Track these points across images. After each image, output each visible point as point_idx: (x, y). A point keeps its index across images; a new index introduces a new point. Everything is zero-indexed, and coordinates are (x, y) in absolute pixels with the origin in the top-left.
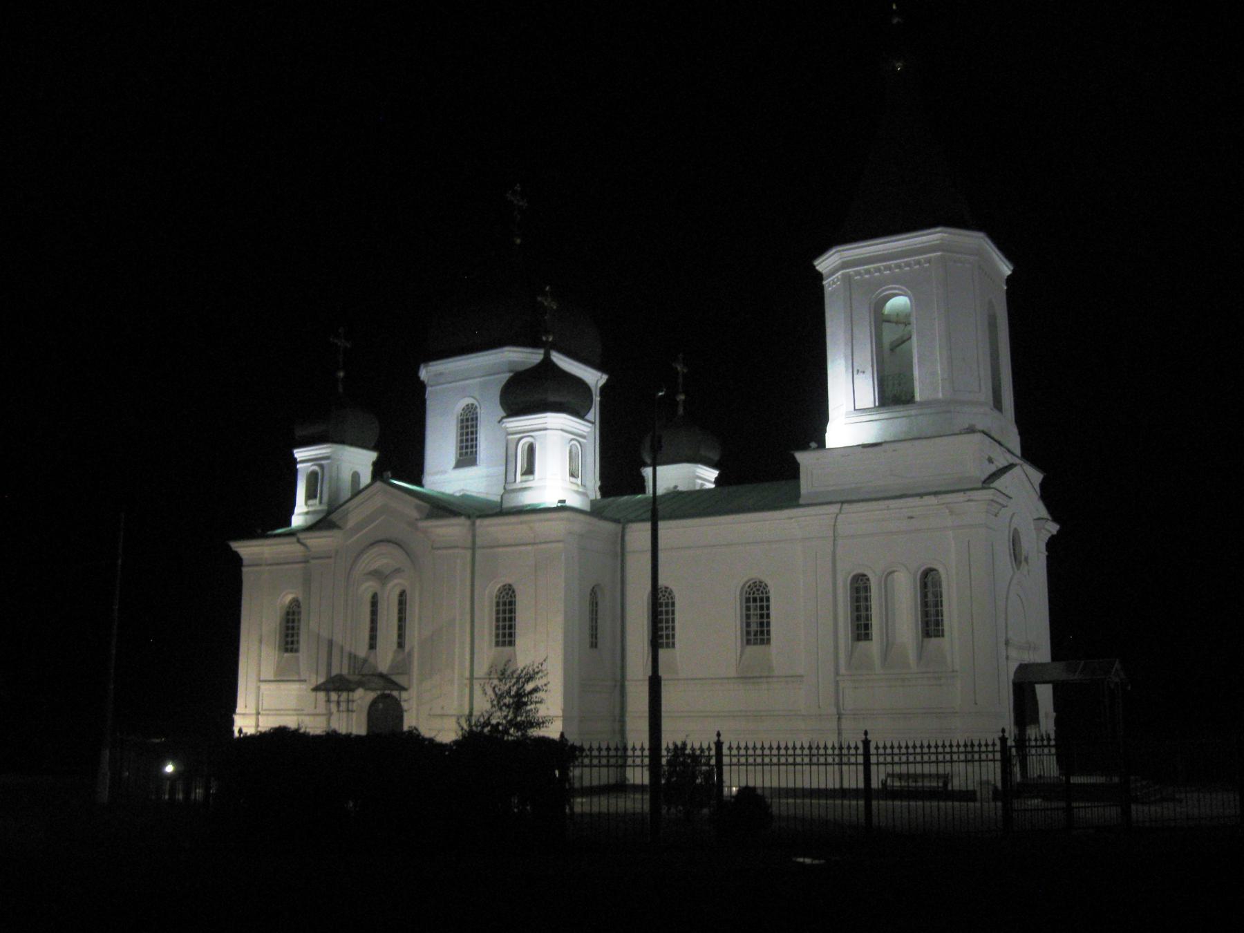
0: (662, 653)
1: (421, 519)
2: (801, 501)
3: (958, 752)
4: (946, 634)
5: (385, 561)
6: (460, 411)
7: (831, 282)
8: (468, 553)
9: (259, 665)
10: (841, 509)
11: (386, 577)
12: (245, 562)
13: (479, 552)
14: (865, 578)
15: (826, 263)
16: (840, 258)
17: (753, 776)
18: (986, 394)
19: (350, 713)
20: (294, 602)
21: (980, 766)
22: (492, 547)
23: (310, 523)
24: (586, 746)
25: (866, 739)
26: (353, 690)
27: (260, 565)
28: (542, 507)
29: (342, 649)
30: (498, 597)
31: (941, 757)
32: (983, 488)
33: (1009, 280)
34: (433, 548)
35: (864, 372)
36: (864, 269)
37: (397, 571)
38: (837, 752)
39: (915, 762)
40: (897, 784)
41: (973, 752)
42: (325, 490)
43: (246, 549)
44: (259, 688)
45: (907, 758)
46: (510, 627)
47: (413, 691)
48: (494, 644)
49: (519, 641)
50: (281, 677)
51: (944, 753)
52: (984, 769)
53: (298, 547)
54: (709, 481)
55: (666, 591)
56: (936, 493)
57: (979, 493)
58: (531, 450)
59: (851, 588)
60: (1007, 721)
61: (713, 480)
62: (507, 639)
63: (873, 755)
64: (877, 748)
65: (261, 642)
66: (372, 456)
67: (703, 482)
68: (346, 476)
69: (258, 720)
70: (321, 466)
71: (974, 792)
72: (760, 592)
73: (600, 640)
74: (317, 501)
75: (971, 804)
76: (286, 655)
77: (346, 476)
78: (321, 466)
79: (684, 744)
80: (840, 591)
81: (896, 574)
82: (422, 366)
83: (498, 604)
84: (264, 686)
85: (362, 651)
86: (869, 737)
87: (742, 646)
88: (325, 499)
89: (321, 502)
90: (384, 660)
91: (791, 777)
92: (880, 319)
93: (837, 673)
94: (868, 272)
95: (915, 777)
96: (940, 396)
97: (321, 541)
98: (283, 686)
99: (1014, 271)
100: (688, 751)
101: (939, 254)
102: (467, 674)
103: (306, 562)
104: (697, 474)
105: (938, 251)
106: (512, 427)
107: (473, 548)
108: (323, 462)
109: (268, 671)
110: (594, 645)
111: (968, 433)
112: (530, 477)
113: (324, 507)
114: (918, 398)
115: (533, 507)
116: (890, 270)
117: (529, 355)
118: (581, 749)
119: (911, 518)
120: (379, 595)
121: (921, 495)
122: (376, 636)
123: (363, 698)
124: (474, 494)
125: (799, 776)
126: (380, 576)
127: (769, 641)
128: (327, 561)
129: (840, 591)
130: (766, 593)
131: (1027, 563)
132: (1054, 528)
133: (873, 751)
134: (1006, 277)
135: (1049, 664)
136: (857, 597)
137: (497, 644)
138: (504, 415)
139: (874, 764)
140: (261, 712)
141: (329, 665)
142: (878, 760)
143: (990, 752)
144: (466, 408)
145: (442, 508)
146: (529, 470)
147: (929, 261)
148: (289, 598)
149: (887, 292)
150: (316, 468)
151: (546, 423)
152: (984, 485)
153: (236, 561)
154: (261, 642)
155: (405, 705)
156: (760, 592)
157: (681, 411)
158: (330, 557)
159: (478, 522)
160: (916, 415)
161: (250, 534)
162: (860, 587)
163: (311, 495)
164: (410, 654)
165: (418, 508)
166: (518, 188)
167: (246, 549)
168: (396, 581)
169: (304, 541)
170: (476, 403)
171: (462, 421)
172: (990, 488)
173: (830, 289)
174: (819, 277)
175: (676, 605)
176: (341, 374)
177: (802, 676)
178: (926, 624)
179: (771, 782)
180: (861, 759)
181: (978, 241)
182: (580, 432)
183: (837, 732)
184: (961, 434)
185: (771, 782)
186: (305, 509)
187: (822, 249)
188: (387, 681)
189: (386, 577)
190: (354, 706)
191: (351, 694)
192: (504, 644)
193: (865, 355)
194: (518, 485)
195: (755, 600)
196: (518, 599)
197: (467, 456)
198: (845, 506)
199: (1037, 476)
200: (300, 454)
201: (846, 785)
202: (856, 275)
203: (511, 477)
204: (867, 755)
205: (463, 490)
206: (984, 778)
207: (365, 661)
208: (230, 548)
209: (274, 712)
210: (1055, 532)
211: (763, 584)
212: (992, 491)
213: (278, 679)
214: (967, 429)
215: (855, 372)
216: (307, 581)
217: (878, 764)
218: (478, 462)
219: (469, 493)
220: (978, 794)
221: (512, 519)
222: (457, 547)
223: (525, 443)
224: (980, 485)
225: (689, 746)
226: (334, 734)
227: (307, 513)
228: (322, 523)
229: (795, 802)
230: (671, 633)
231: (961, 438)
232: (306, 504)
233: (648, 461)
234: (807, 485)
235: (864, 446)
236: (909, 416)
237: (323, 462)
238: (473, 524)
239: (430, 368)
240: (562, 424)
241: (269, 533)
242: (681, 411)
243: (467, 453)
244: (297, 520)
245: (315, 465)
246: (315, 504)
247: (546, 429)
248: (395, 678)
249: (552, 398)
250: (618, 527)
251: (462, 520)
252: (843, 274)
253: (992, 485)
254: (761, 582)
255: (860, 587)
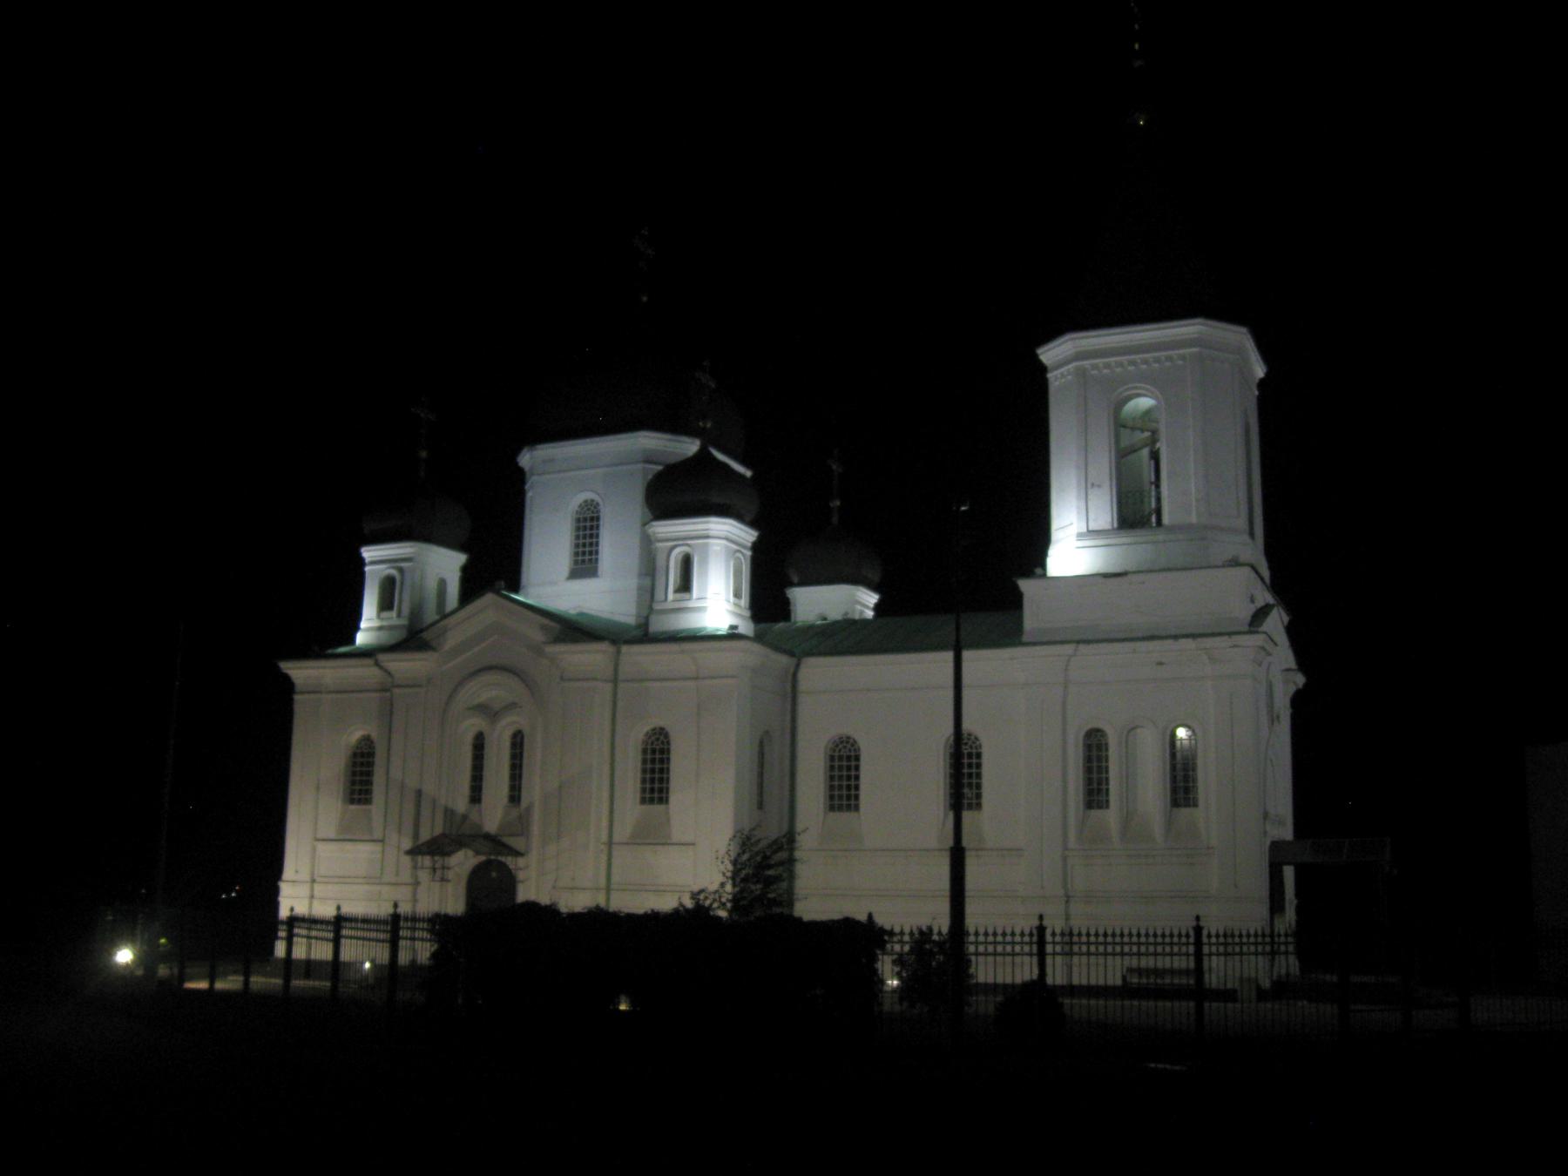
0: (967, 816)
1: (549, 643)
2: (1025, 638)
3: (986, 943)
4: (1201, 802)
5: (494, 693)
6: (576, 508)
7: (1066, 373)
8: (609, 687)
9: (316, 819)
10: (1075, 650)
11: (496, 714)
12: (298, 688)
13: (621, 685)
14: (1100, 734)
15: (1049, 354)
16: (1074, 347)
17: (1011, 970)
18: (1242, 522)
19: (444, 883)
20: (364, 740)
21: (1241, 961)
22: (642, 680)
23: (393, 641)
24: (897, 930)
25: (1041, 924)
26: (449, 854)
27: (320, 692)
28: (703, 633)
29: (434, 802)
30: (645, 742)
31: (1126, 949)
32: (1251, 632)
33: (1262, 384)
34: (562, 679)
35: (1099, 486)
36: (1140, 358)
37: (512, 706)
38: (1268, 939)
39: (1147, 954)
40: (1135, 980)
41: (1071, 943)
42: (405, 600)
43: (300, 672)
44: (314, 850)
45: (1013, 948)
46: (661, 780)
47: (533, 858)
48: (638, 800)
49: (675, 797)
50: (346, 835)
51: (1131, 944)
52: (1245, 964)
53: (375, 671)
54: (867, 607)
55: (847, 742)
56: (1194, 636)
57: (1246, 637)
58: (687, 564)
59: (1084, 745)
60: (1263, 911)
61: (872, 606)
62: (656, 795)
63: (1205, 944)
64: (1209, 936)
65: (318, 788)
66: (460, 558)
67: (862, 608)
68: (431, 585)
69: (312, 890)
70: (401, 570)
71: (1235, 991)
72: (660, 742)
73: (485, 792)
74: (394, 614)
75: (1230, 1005)
76: (353, 807)
77: (431, 585)
78: (401, 570)
79: (930, 929)
80: (1071, 751)
81: (1138, 731)
82: (525, 450)
83: (644, 751)
84: (321, 846)
85: (461, 804)
86: (1045, 923)
87: (825, 813)
88: (406, 610)
89: (399, 615)
90: (493, 815)
91: (1009, 970)
92: (1120, 425)
93: (1066, 848)
94: (1107, 366)
95: (1157, 972)
96: (1194, 519)
97: (405, 665)
98: (349, 846)
99: (1267, 374)
100: (936, 937)
101: (1195, 350)
102: (604, 837)
103: (384, 690)
104: (858, 598)
105: (1194, 346)
106: (662, 533)
107: (615, 681)
108: (403, 565)
109: (328, 828)
110: (761, 806)
111: (1231, 566)
112: (686, 595)
113: (404, 622)
114: (1166, 520)
115: (692, 634)
116: (1135, 366)
117: (668, 444)
118: (891, 933)
119: (1161, 664)
120: (486, 735)
121: (1176, 637)
122: (981, 793)
123: (463, 862)
124: (593, 613)
125: (1000, 970)
126: (489, 712)
127: (857, 808)
128: (417, 690)
129: (1071, 751)
130: (976, 748)
131: (1279, 722)
132: (1300, 680)
133: (1049, 938)
134: (1257, 381)
135: (1288, 843)
136: (1089, 756)
137: (643, 801)
138: (651, 517)
139: (1206, 955)
140: (318, 879)
141: (417, 825)
142: (1054, 950)
143: (1167, 944)
144: (583, 504)
145: (574, 630)
146: (685, 585)
147: (1183, 358)
148: (356, 735)
149: (1128, 393)
150: (393, 572)
151: (707, 530)
152: (1252, 629)
153: (286, 687)
154: (318, 788)
155: (521, 875)
156: (660, 742)
157: (835, 520)
158: (420, 686)
159: (625, 649)
160: (1165, 541)
161: (306, 652)
162: (1095, 745)
163: (386, 604)
164: (529, 809)
165: (543, 628)
166: (645, 232)
167: (300, 672)
168: (515, 718)
169: (385, 664)
170: (599, 500)
171: (578, 520)
172: (1257, 632)
173: (1057, 383)
174: (1042, 369)
175: (862, 758)
176: (424, 454)
177: (1019, 850)
178: (1174, 790)
179: (1013, 977)
180: (1191, 949)
181: (1238, 338)
182: (734, 537)
183: (1064, 917)
184: (1223, 566)
185: (1013, 977)
186: (376, 623)
187: (1052, 333)
188: (496, 843)
189: (496, 714)
190: (450, 875)
191: (446, 859)
192: (652, 801)
193: (1103, 465)
194: (669, 605)
195: (841, 758)
196: (673, 747)
197: (585, 563)
198: (1082, 647)
199: (1286, 619)
200: (368, 553)
201: (1076, 981)
202: (1093, 370)
203: (659, 595)
204: (1198, 943)
205: (579, 607)
206: (1246, 975)
207: (465, 817)
208: (278, 669)
209: (336, 880)
210: (1301, 686)
211: (973, 737)
212: (1262, 637)
213: (341, 837)
214: (1230, 561)
215: (1089, 486)
216: (387, 713)
217: (1054, 954)
218: (600, 573)
219: (585, 611)
220: (1239, 994)
221: (674, 647)
222: (595, 679)
223: (679, 553)
224: (1246, 628)
225: (936, 930)
226: (553, 907)
227: (380, 628)
228: (413, 638)
229: (212, 983)
230: (1104, 798)
231: (1224, 570)
232: (379, 616)
233: (796, 579)
234: (1032, 619)
235: (1106, 576)
236: (1154, 543)
237: (403, 565)
238: (619, 652)
239: (535, 453)
240: (728, 532)
241: (330, 651)
242: (835, 520)
243: (583, 561)
244: (361, 639)
245: (393, 568)
246: (392, 617)
247: (707, 537)
248: (506, 840)
249: (716, 499)
250: (793, 661)
251: (604, 646)
252: (1077, 369)
253: (1261, 629)
254: (976, 739)
255: (1095, 745)
